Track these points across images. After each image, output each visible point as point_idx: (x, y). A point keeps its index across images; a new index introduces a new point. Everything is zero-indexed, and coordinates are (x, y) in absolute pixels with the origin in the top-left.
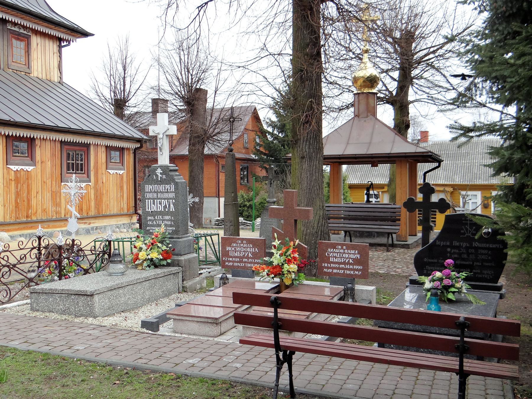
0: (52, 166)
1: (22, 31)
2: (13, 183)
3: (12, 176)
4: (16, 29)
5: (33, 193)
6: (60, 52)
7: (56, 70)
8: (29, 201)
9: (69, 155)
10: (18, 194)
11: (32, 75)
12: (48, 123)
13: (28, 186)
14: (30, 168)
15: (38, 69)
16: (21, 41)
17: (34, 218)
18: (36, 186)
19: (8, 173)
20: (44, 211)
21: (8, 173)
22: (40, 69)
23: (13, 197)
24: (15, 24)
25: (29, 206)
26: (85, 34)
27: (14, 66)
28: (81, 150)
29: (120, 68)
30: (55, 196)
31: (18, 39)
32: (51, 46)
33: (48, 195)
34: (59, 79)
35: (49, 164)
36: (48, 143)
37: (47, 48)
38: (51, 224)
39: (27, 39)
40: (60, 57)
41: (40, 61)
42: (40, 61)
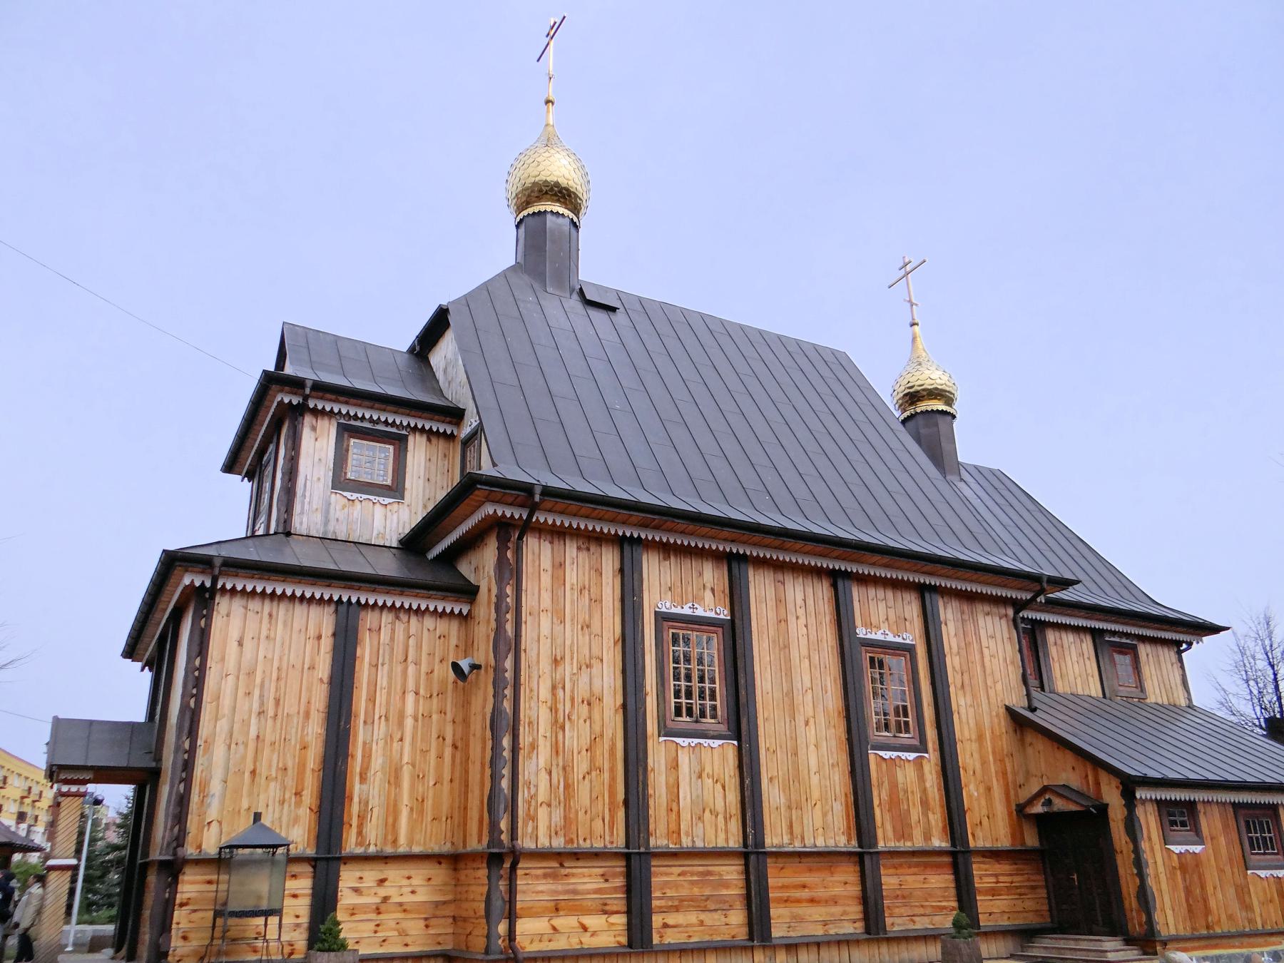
0: (1227, 844)
1: (1124, 640)
2: (1178, 872)
3: (1176, 863)
4: (1117, 639)
5: (1210, 890)
6: (1181, 660)
7: (1180, 688)
8: (1205, 900)
9: (1247, 823)
10: (1188, 892)
11: (1148, 701)
12: (1172, 775)
13: (1200, 878)
14: (1197, 849)
15: (1154, 694)
16: (1126, 654)
17: (1218, 931)
18: (1211, 877)
19: (1169, 857)
20: (1230, 917)
21: (1169, 857)
22: (1157, 691)
23: (1183, 895)
24: (1114, 633)
25: (1207, 911)
26: (1214, 629)
27: (1124, 691)
28: (1264, 815)
29: (1262, 664)
30: (1242, 892)
31: (1120, 653)
32: (1167, 655)
33: (1231, 892)
34: (274, 613)
35: (1222, 840)
36: (1215, 808)
37: (1162, 658)
38: (1246, 940)
39: (1132, 651)
40: (1182, 667)
41: (1155, 678)
42: (1155, 678)
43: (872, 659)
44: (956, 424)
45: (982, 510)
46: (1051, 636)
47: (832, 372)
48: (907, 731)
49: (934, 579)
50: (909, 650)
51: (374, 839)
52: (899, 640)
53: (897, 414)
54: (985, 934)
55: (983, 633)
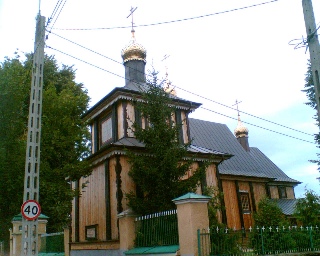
32: (291, 189)
43: (242, 196)
44: (248, 139)
45: (255, 159)
46: (270, 187)
47: (223, 128)
48: (248, 209)
49: (252, 181)
50: (248, 194)
51: (207, 236)
52: (246, 192)
53: (236, 137)
54: (113, 241)
55: (260, 189)
